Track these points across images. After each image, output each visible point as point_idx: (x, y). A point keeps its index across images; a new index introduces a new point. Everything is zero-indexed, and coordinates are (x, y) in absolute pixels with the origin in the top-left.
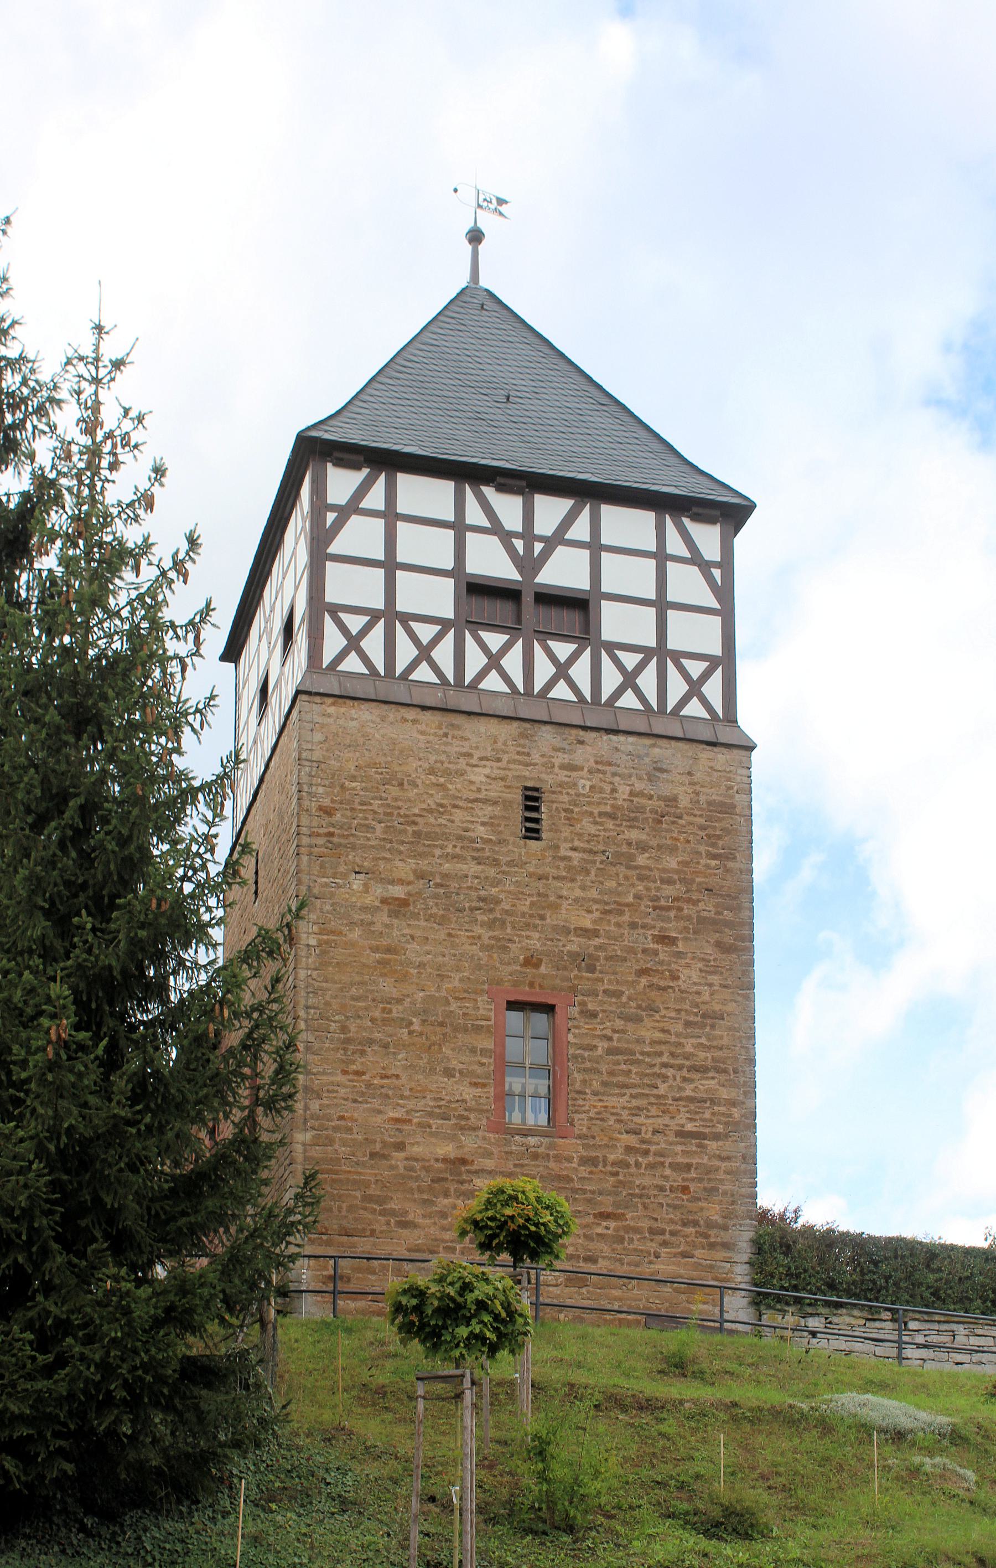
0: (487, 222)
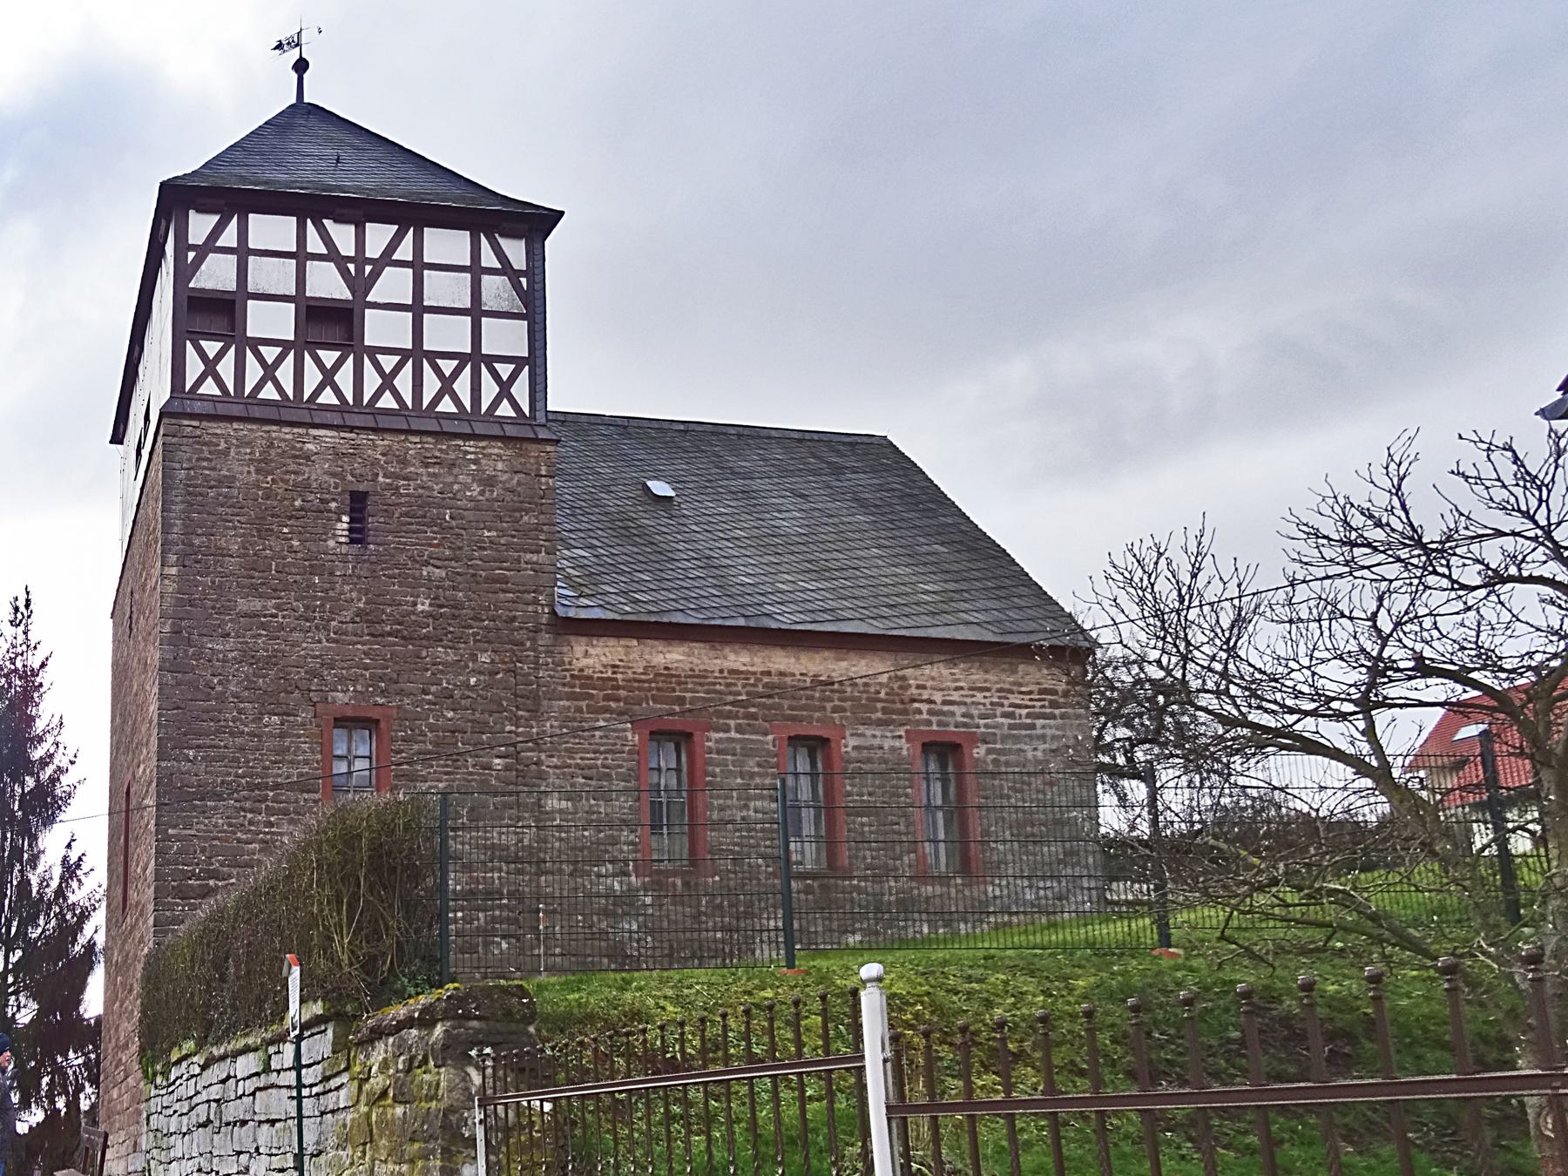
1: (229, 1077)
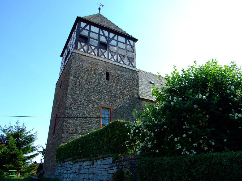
0: (101, 7)
1: (82, 165)
